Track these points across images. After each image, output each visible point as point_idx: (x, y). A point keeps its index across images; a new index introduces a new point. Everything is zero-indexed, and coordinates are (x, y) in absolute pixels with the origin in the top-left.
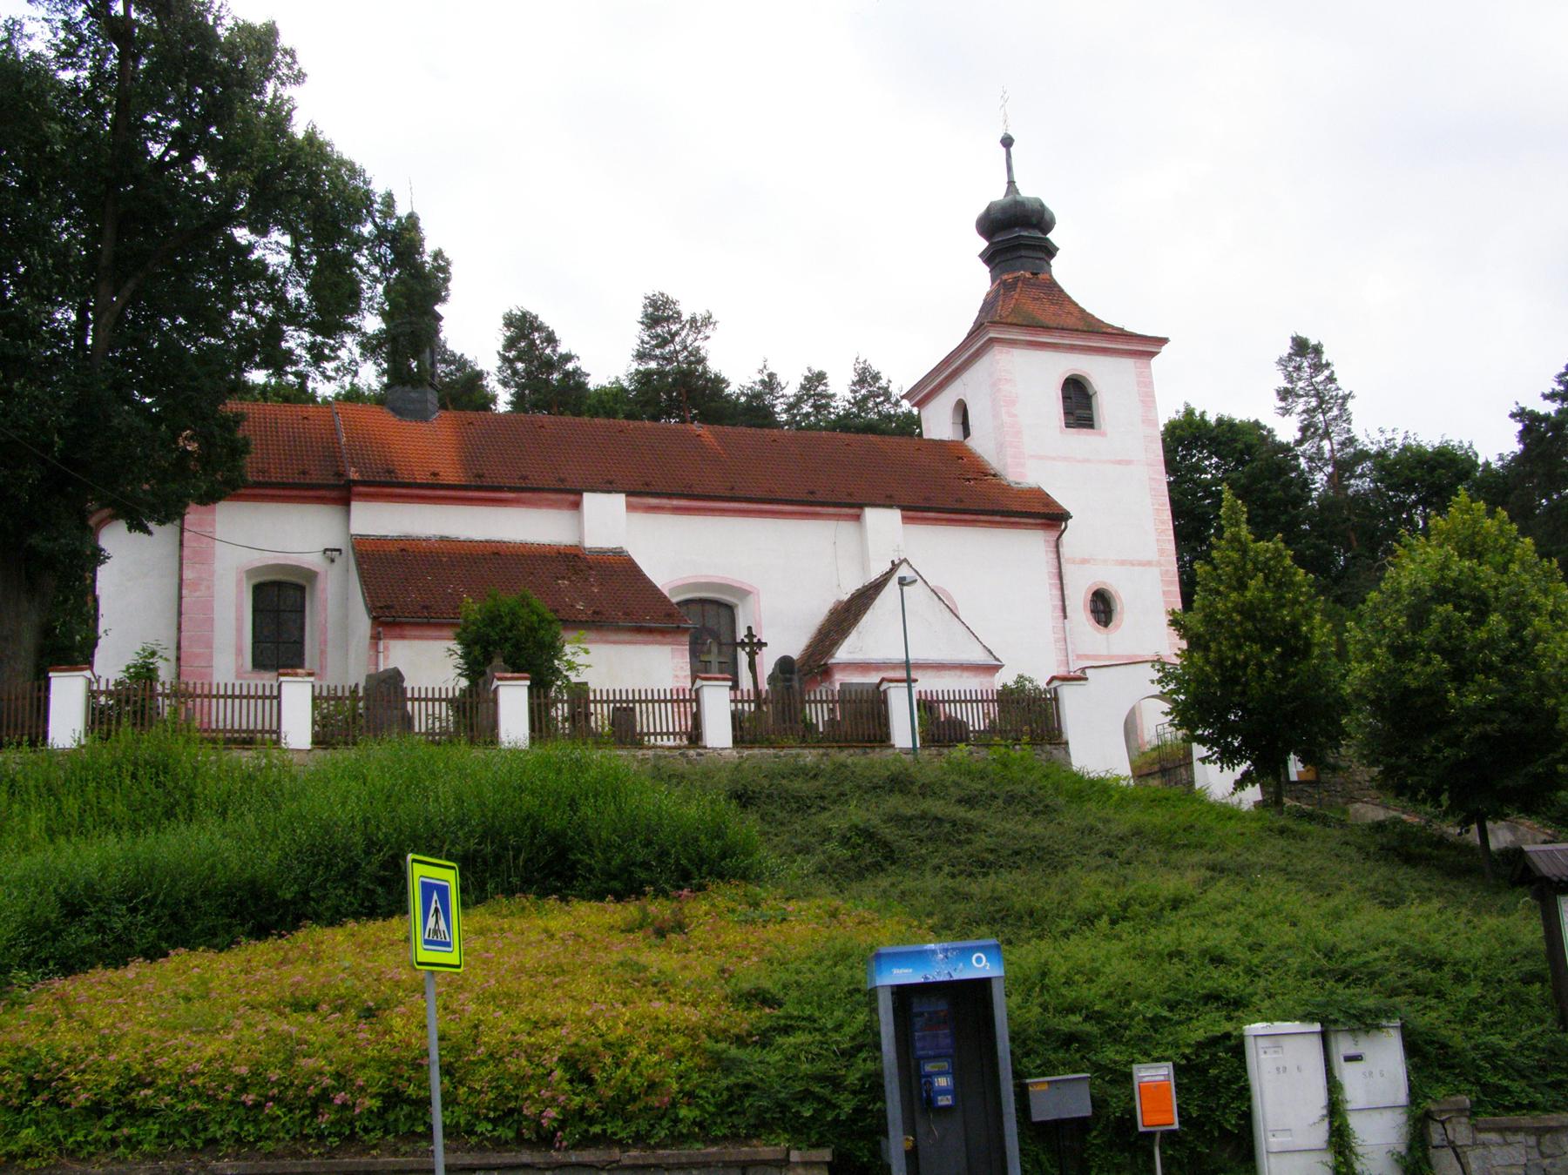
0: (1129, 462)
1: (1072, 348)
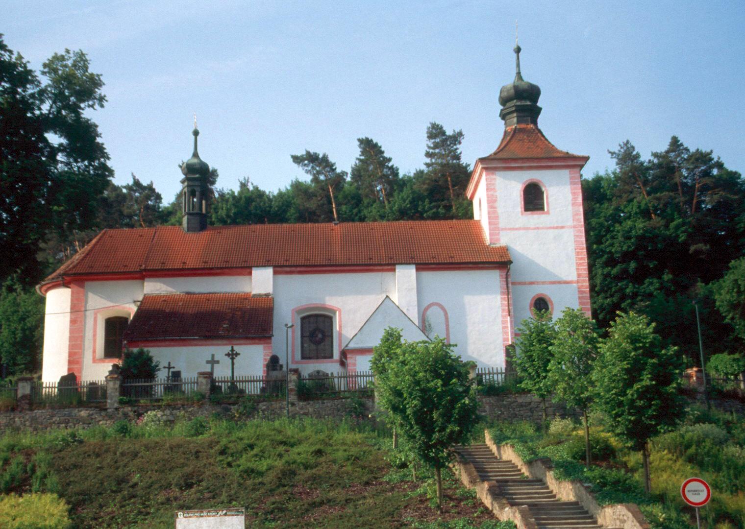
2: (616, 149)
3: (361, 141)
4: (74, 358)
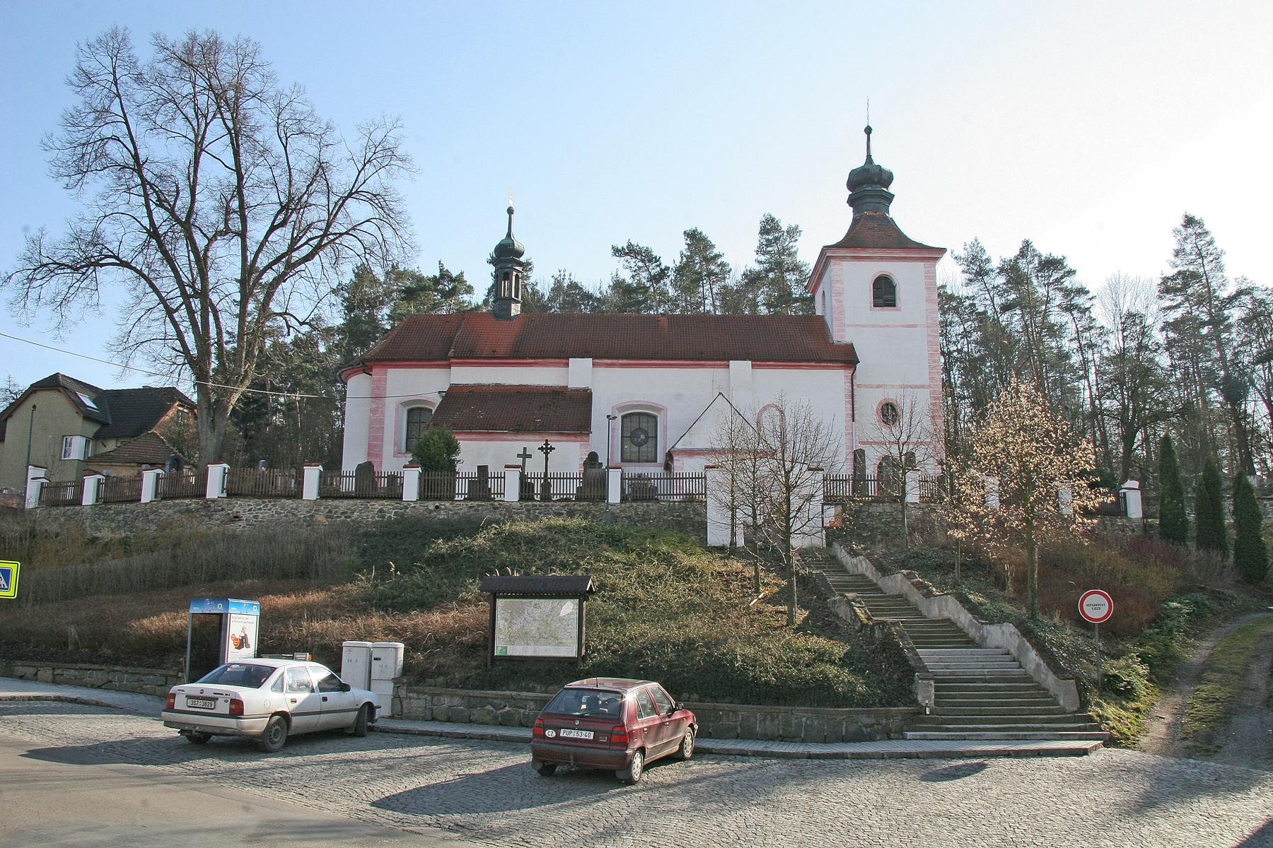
0: (915, 326)
1: (882, 259)
2: (963, 254)
3: (686, 234)
4: (374, 447)
